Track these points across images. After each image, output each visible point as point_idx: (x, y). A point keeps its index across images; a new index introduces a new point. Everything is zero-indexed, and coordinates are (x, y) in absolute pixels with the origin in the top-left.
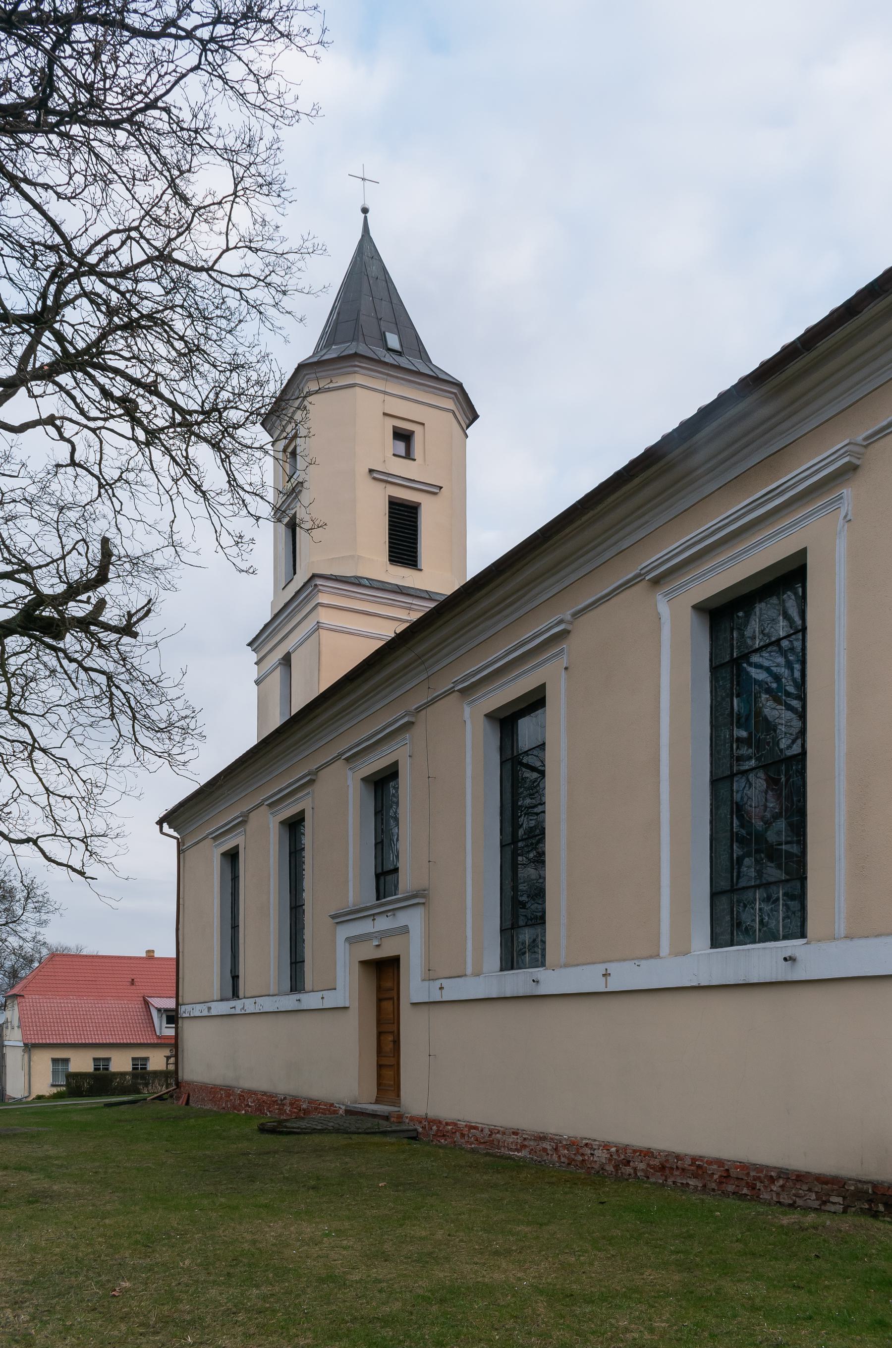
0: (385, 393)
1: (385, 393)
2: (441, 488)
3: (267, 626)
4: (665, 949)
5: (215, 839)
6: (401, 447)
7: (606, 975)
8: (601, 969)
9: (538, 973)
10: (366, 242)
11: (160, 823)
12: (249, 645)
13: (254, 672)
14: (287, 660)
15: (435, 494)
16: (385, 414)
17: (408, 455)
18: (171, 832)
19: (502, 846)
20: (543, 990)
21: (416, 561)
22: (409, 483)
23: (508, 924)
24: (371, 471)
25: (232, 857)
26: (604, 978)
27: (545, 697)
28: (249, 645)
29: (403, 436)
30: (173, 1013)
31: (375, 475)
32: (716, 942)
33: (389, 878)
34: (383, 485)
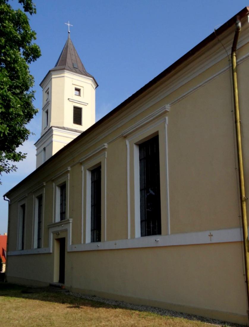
0: (73, 79)
1: (73, 79)
2: (88, 104)
3: (39, 140)
4: (170, 233)
5: (19, 201)
6: (78, 92)
7: (211, 235)
8: (208, 233)
9: (158, 238)
10: (68, 41)
11: (4, 196)
12: (35, 145)
13: (35, 152)
14: (44, 149)
15: (86, 105)
16: (73, 84)
17: (79, 95)
18: (7, 199)
19: (92, 206)
20: (100, 248)
21: (81, 123)
22: (79, 102)
23: (93, 229)
24: (69, 99)
25: (23, 207)
26: (210, 237)
27: (66, 184)
28: (35, 145)
29: (78, 90)
30: (17, 249)
31: (70, 100)
32: (159, 233)
33: (64, 215)
34: (72, 102)
